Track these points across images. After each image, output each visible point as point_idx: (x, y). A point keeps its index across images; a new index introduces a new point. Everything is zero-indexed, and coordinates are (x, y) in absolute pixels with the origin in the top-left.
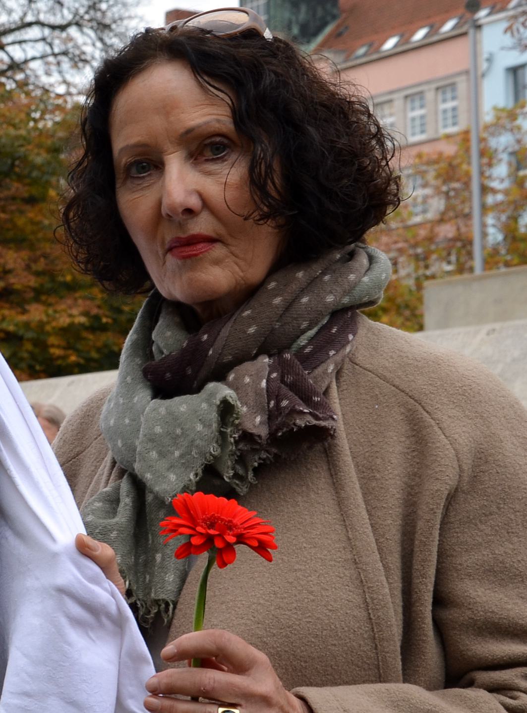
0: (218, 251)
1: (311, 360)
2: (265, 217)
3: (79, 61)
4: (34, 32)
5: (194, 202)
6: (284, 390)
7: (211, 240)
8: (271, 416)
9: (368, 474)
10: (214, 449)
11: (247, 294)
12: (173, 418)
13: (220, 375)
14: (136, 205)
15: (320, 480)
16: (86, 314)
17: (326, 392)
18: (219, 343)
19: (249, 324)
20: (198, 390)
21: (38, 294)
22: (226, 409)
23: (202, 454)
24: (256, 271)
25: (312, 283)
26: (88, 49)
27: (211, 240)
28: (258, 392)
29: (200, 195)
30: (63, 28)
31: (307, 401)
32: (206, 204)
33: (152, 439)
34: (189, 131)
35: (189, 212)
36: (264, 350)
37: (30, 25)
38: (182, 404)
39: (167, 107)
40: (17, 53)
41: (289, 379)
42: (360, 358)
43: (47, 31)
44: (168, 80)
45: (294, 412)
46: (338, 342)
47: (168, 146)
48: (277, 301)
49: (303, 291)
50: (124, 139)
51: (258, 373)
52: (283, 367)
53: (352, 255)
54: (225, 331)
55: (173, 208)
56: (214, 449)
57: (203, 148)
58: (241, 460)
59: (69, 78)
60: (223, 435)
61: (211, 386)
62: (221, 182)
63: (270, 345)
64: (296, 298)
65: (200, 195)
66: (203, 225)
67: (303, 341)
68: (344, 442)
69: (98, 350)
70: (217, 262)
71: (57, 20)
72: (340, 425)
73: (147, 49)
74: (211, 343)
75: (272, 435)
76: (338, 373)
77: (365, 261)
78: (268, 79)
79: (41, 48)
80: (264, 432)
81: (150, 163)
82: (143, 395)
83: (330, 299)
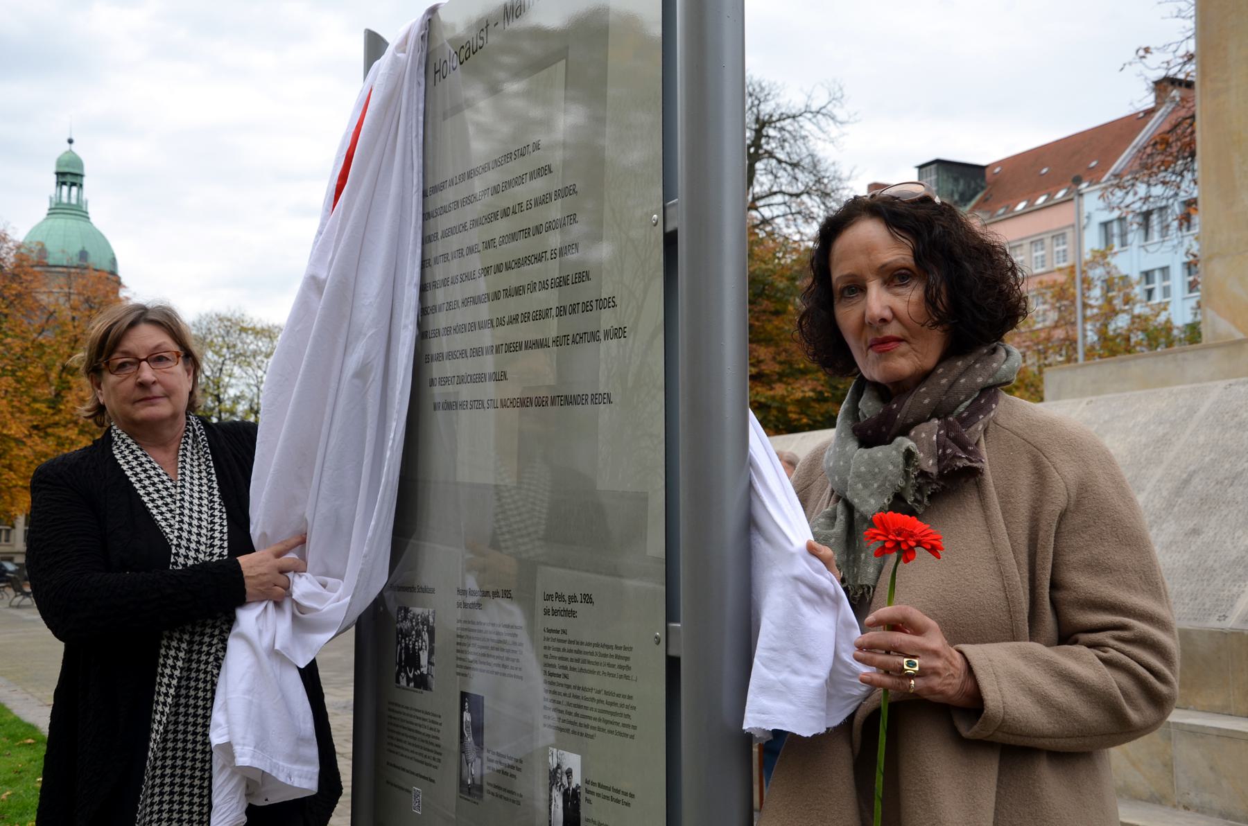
0: (903, 347)
1: (967, 421)
2: (935, 324)
3: (809, 218)
4: (778, 199)
5: (887, 314)
6: (949, 442)
7: (899, 340)
8: (940, 460)
9: (1005, 499)
10: (901, 482)
11: (923, 377)
12: (873, 461)
13: (905, 432)
14: (847, 316)
15: (973, 504)
16: (813, 390)
17: (977, 444)
18: (904, 410)
19: (925, 397)
20: (890, 442)
21: (781, 377)
22: (909, 455)
23: (893, 485)
24: (930, 361)
25: (967, 370)
26: (815, 210)
27: (899, 340)
28: (930, 444)
29: (891, 309)
30: (798, 195)
31: (964, 448)
32: (895, 315)
33: (858, 475)
34: (884, 266)
35: (884, 321)
36: (935, 415)
37: (775, 193)
38: (879, 452)
39: (868, 250)
40: (767, 213)
41: (952, 435)
42: (1000, 421)
43: (787, 198)
44: (869, 231)
45: (955, 457)
46: (985, 409)
47: (869, 276)
48: (944, 381)
49: (961, 375)
50: (839, 272)
51: (931, 431)
52: (947, 426)
53: (994, 350)
54: (908, 402)
55: (873, 318)
56: (901, 482)
57: (893, 277)
58: (919, 489)
59: (802, 229)
60: (907, 473)
61: (899, 439)
62: (907, 300)
63: (939, 411)
64: (957, 379)
65: (891, 309)
66: (893, 330)
67: (961, 409)
68: (989, 478)
69: (822, 415)
70: (903, 355)
71: (794, 190)
72: (986, 466)
73: (855, 210)
74: (899, 410)
75: (940, 473)
76: (986, 431)
77: (1004, 354)
78: (938, 230)
79: (783, 209)
80: (934, 470)
81: (857, 287)
82: (852, 446)
83: (980, 380)
